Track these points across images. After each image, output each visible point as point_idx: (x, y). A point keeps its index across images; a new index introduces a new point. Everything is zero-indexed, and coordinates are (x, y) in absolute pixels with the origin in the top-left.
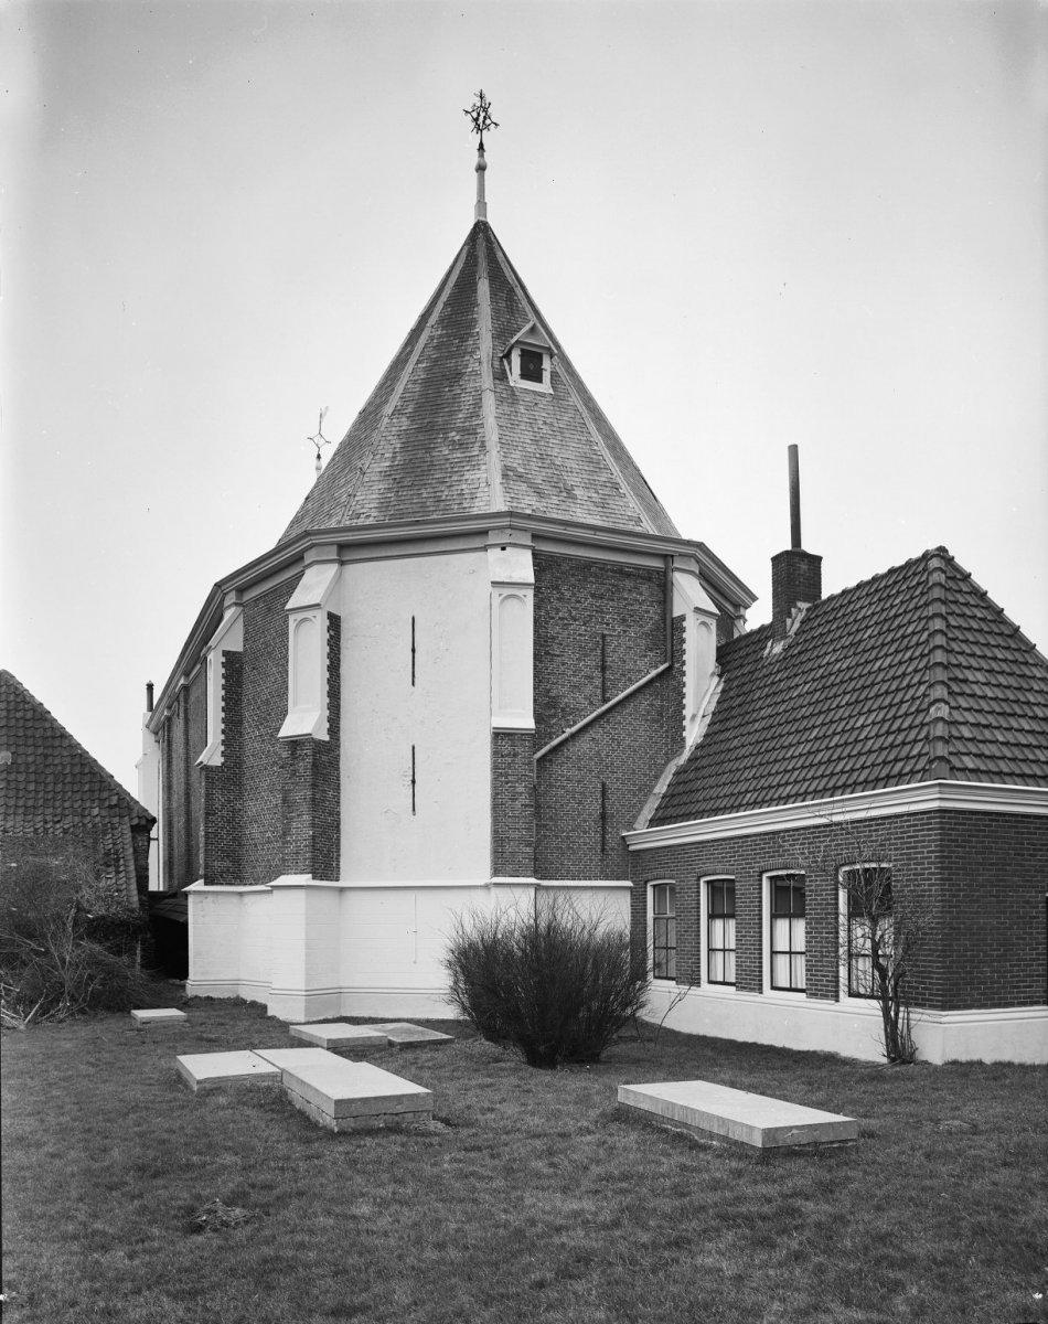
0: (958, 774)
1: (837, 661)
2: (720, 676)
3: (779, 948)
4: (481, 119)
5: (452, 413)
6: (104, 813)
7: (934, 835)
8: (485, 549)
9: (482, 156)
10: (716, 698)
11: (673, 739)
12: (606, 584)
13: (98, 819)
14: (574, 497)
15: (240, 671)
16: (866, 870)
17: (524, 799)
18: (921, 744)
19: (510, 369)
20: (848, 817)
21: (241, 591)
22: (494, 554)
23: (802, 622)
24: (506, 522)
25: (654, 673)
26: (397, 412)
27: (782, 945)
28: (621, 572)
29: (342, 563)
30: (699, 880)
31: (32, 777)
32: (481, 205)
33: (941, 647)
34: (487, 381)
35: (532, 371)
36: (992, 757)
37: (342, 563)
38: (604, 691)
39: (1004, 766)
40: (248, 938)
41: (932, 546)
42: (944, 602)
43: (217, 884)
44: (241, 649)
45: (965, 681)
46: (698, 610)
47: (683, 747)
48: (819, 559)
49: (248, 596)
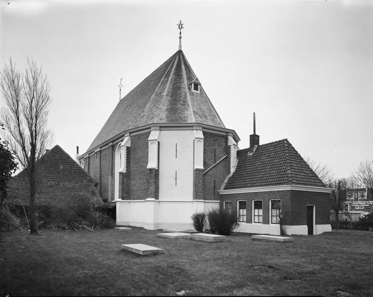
0: (293, 183)
1: (266, 159)
2: (237, 158)
3: (255, 215)
4: (180, 26)
5: (180, 97)
6: (87, 182)
7: (290, 194)
8: (193, 130)
9: (180, 35)
10: (237, 163)
11: (228, 171)
12: (216, 138)
13: (86, 183)
14: (207, 118)
15: (130, 151)
16: (278, 200)
17: (202, 183)
18: (286, 178)
19: (192, 87)
20: (276, 190)
21: (130, 133)
22: (195, 131)
23: (256, 149)
24: (198, 125)
25: (224, 157)
26: (167, 95)
27: (241, 214)
28: (219, 136)
29: (160, 130)
30: (237, 201)
31: (69, 172)
32: (180, 46)
33: (288, 159)
34: (187, 90)
35: (196, 89)
36: (298, 180)
37: (160, 130)
38: (215, 161)
39: (300, 182)
40: (132, 213)
41: (285, 138)
42: (288, 150)
43: (124, 200)
44: (130, 146)
45: (293, 166)
46: (234, 145)
47: (230, 173)
48: (259, 136)
49: (132, 134)
